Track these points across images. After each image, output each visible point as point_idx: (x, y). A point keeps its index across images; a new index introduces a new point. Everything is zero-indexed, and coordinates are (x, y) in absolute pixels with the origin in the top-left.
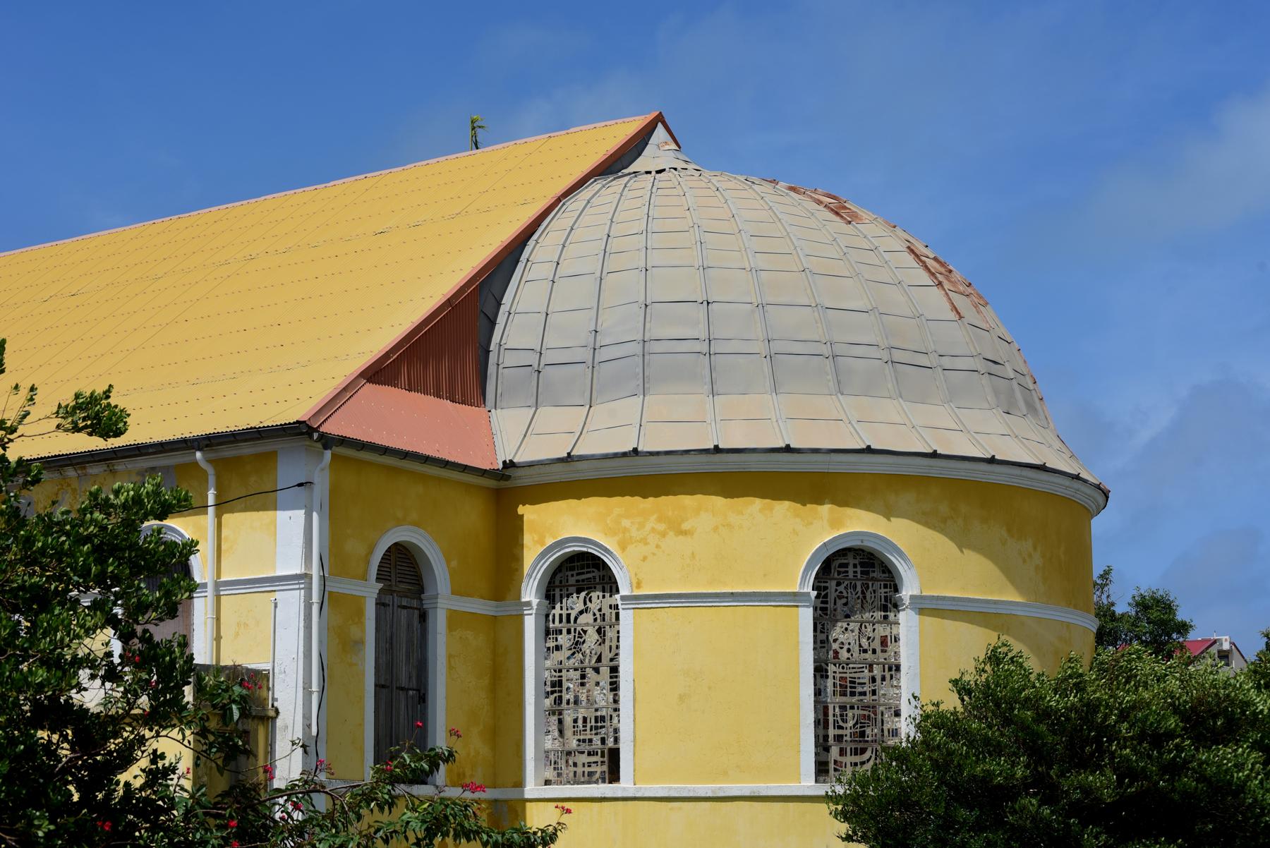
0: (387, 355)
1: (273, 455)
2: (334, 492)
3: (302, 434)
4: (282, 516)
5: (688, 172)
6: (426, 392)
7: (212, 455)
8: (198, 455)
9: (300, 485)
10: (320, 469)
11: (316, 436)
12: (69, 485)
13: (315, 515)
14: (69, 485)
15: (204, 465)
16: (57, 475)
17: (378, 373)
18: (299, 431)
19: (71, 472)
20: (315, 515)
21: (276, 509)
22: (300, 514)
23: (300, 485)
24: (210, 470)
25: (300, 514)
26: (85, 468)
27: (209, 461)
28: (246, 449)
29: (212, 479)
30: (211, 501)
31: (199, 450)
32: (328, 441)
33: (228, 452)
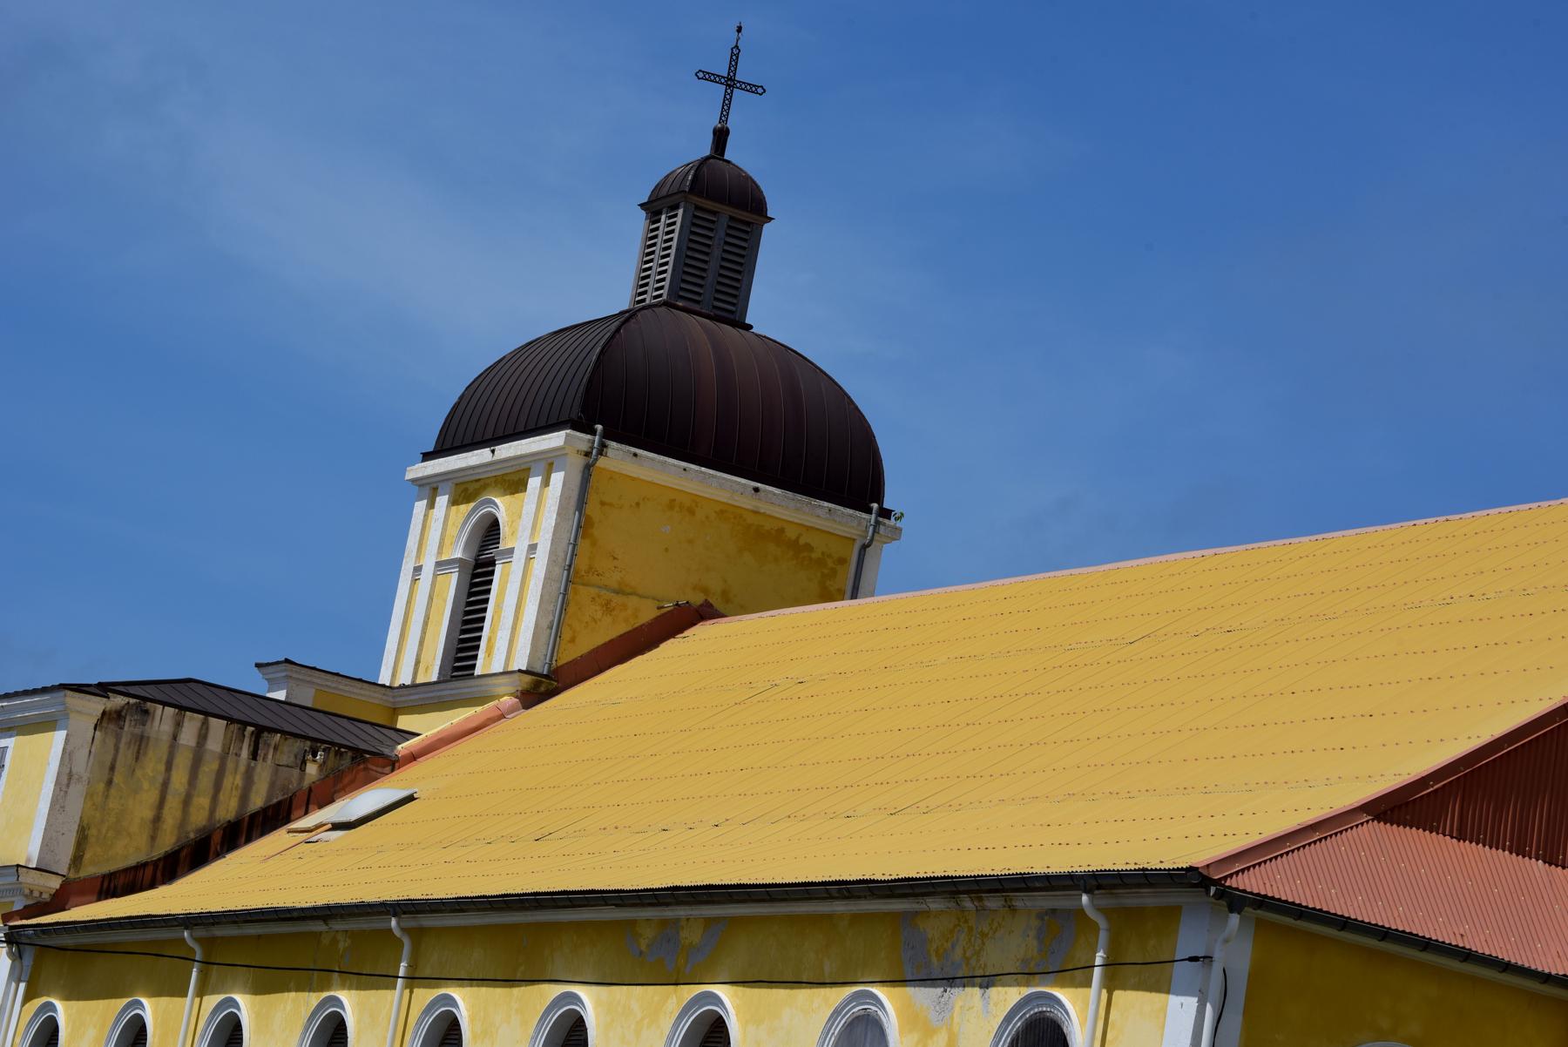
0: (1423, 782)
1: (1171, 914)
2: (1256, 978)
3: (1195, 886)
4: (1174, 1000)
5: (819, 512)
6: (1494, 843)
7: (1107, 901)
8: (1085, 898)
9: (1193, 959)
10: (1233, 947)
11: (1213, 889)
12: (966, 921)
13: (1209, 1007)
14: (966, 921)
15: (1091, 914)
16: (952, 904)
17: (1397, 808)
18: (1192, 879)
19: (993, 902)
20: (1209, 1007)
21: (1168, 992)
22: (1192, 1002)
23: (1193, 959)
24: (1102, 923)
25: (1192, 1002)
26: (980, 899)
27: (1099, 909)
28: (1149, 899)
29: (1103, 937)
30: (1098, 961)
31: (1086, 892)
32: (1236, 901)
33: (1131, 900)
